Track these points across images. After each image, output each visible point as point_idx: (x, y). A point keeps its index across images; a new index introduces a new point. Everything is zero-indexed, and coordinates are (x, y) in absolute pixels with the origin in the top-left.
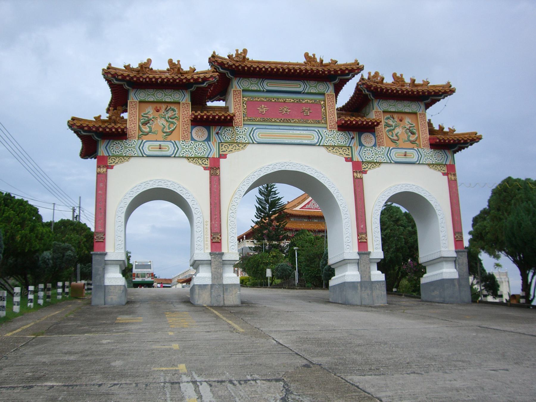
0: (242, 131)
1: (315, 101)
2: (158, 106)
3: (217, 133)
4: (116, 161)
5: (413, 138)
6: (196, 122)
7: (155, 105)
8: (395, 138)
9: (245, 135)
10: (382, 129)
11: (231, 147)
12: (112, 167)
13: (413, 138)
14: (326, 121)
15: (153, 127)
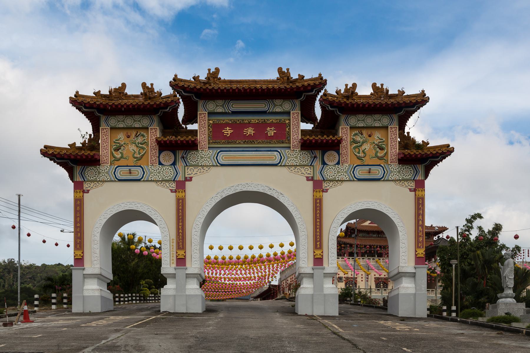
0: (205, 153)
2: (129, 132)
3: (183, 157)
4: (92, 186)
5: (381, 154)
6: (163, 146)
7: (125, 132)
8: (361, 155)
9: (209, 158)
10: (346, 147)
11: (196, 170)
13: (381, 154)
14: (289, 140)
15: (125, 152)
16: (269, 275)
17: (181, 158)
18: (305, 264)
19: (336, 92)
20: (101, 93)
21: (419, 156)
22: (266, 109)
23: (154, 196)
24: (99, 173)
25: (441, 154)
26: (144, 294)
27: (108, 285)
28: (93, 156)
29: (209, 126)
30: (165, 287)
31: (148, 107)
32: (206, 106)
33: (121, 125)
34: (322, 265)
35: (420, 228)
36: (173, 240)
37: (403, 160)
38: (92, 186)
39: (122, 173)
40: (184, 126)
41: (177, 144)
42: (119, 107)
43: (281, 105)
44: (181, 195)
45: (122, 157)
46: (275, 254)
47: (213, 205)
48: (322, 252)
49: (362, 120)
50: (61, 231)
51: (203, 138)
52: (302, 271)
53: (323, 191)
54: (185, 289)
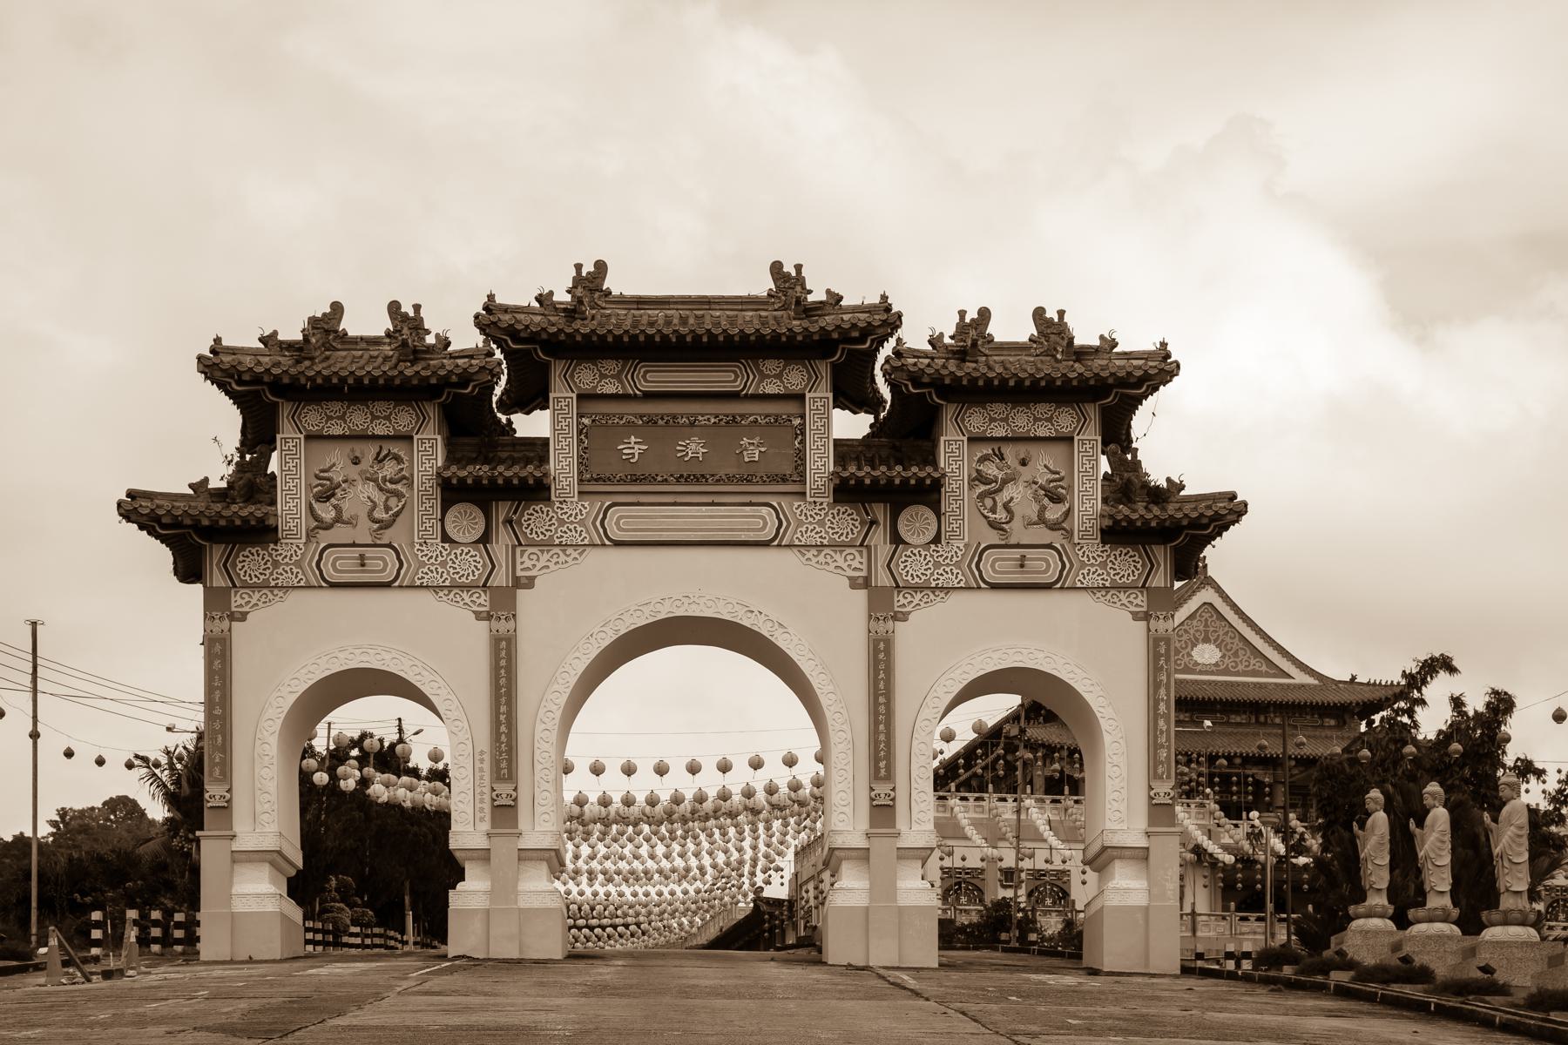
0: (570, 507)
1: (777, 417)
3: (509, 522)
4: (254, 601)
5: (1054, 512)
6: (451, 493)
8: (1001, 515)
11: (546, 556)
12: (243, 617)
15: (345, 506)
16: (755, 861)
17: (504, 523)
18: (847, 822)
19: (930, 342)
20: (280, 337)
21: (1153, 524)
22: (737, 386)
23: (426, 633)
24: (276, 564)
25: (1212, 519)
26: (335, 924)
27: (290, 880)
28: (261, 520)
29: (580, 432)
30: (460, 886)
31: (415, 382)
32: (572, 376)
33: (337, 430)
34: (516, 827)
35: (1161, 723)
36: (482, 753)
37: (1115, 534)
38: (254, 601)
39: (340, 565)
40: (504, 418)
41: (492, 483)
42: (335, 381)
43: (779, 376)
44: (503, 626)
45: (338, 519)
46: (771, 790)
47: (593, 656)
48: (893, 789)
49: (1002, 420)
50: (169, 729)
51: (562, 467)
52: (839, 841)
53: (895, 618)
54: (516, 892)
